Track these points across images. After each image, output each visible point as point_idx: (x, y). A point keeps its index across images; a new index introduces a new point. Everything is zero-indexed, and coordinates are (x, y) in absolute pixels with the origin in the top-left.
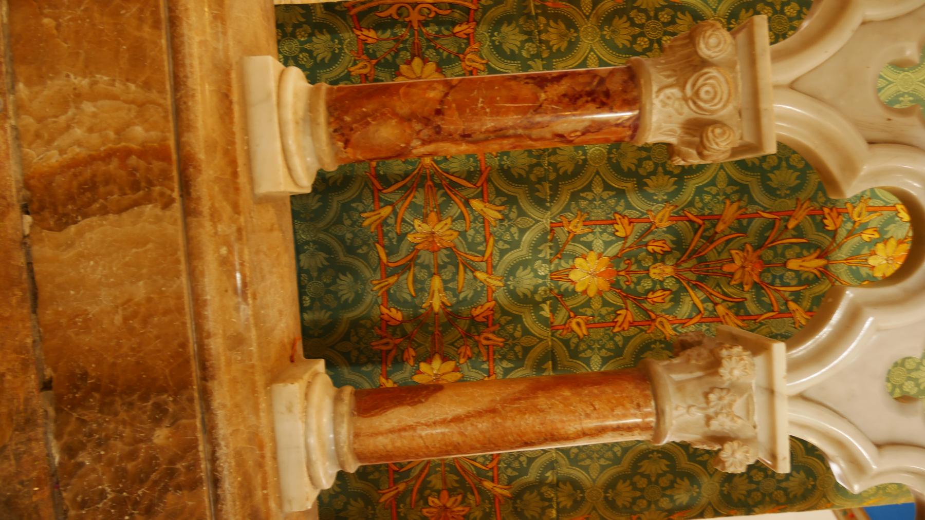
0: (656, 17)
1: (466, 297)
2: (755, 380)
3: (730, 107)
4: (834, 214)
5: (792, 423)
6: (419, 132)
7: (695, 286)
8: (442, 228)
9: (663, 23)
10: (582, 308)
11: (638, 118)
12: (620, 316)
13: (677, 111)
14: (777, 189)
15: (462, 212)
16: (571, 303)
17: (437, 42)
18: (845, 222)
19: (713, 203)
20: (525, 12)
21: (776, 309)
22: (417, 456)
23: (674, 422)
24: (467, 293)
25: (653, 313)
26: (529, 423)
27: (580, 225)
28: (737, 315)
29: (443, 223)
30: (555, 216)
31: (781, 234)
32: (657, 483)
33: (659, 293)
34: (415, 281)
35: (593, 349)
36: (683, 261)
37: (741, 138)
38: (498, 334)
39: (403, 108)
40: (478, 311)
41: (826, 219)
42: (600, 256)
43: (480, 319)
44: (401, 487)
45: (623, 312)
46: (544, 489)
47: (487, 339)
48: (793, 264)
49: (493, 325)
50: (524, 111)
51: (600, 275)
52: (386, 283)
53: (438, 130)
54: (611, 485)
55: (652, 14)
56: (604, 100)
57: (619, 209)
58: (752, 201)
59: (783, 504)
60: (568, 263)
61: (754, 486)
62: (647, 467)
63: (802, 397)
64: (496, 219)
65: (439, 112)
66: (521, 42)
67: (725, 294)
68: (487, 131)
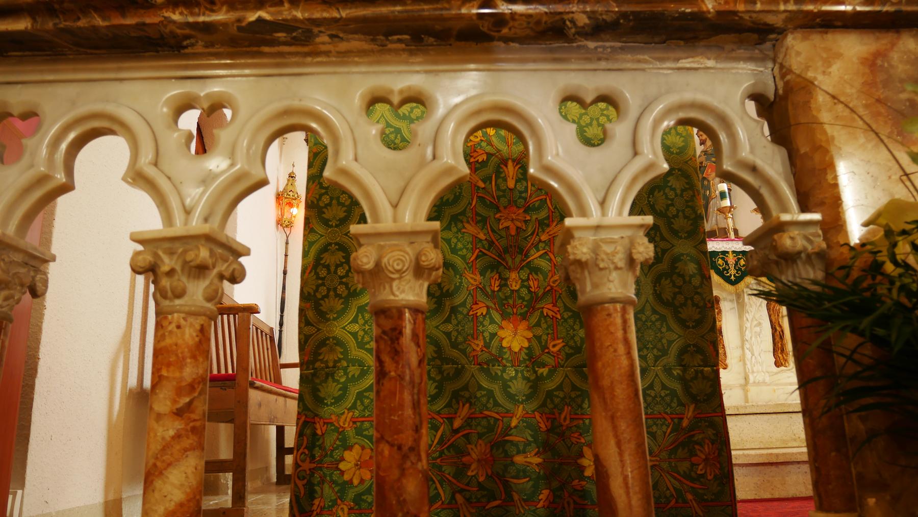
0: (323, 279)
1: (531, 435)
2: (590, 237)
3: (408, 249)
4: (475, 154)
5: (620, 213)
6: (413, 463)
7: (526, 255)
8: (475, 453)
9: (328, 274)
10: (542, 343)
11: (410, 309)
12: (549, 314)
13: (407, 283)
14: (455, 194)
15: (463, 436)
16: (537, 351)
17: (327, 448)
18: (481, 147)
19: (463, 242)
20: (310, 377)
21: (544, 197)
22: (646, 475)
23: (620, 291)
24: (528, 435)
25: (546, 288)
26: (621, 392)
27: (477, 342)
28: (548, 226)
29: (470, 451)
30: (469, 361)
31: (489, 193)
32: (680, 287)
33: (531, 283)
34: (517, 477)
35: (574, 335)
36: (507, 264)
37: (428, 242)
38: (562, 410)
39: (396, 473)
40: (542, 425)
41: (478, 160)
42: (501, 328)
43: (549, 424)
44: (689, 497)
45: (545, 311)
46: (688, 377)
47: (565, 419)
48: (511, 184)
49: (554, 414)
50: (402, 387)
51: (516, 328)
52: (518, 501)
53: (412, 449)
54: (683, 323)
55: (320, 282)
56: (397, 332)
57: (465, 312)
58: (463, 213)
59: (694, 193)
60: (506, 352)
61: (680, 214)
62: (667, 295)
63: (603, 203)
64: (470, 408)
65: (400, 448)
66: (333, 382)
67: (532, 234)
68: (414, 414)
